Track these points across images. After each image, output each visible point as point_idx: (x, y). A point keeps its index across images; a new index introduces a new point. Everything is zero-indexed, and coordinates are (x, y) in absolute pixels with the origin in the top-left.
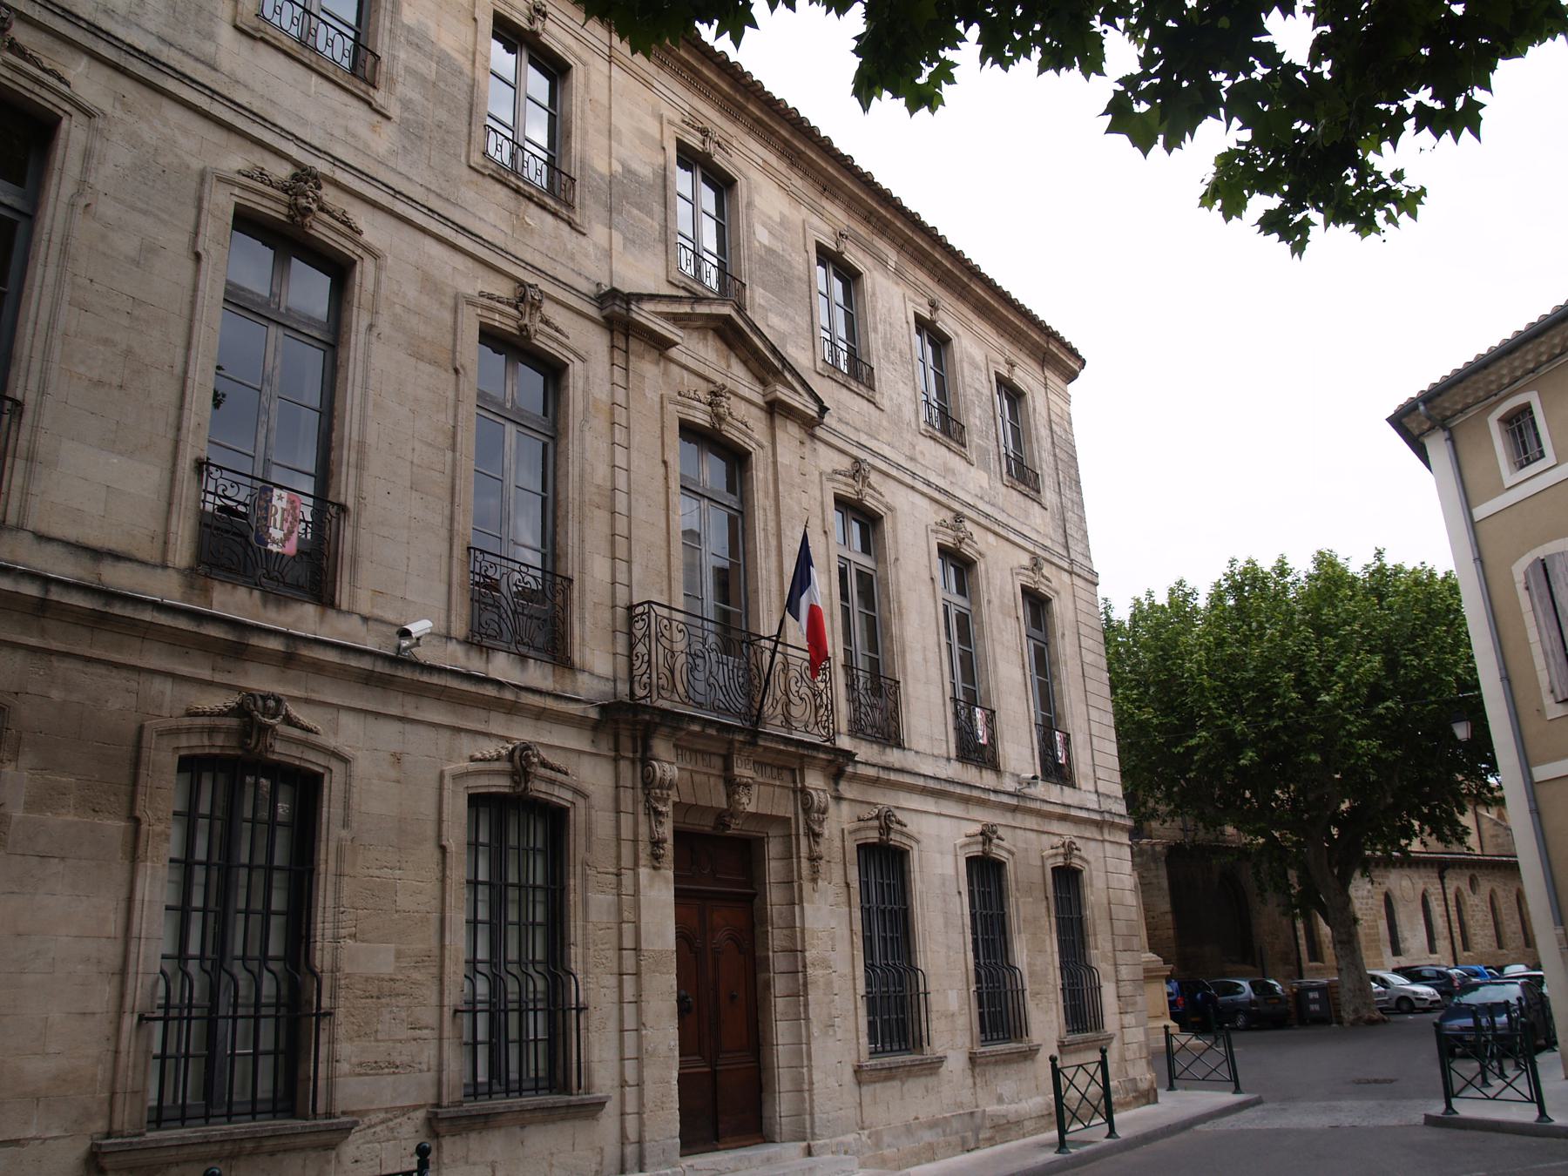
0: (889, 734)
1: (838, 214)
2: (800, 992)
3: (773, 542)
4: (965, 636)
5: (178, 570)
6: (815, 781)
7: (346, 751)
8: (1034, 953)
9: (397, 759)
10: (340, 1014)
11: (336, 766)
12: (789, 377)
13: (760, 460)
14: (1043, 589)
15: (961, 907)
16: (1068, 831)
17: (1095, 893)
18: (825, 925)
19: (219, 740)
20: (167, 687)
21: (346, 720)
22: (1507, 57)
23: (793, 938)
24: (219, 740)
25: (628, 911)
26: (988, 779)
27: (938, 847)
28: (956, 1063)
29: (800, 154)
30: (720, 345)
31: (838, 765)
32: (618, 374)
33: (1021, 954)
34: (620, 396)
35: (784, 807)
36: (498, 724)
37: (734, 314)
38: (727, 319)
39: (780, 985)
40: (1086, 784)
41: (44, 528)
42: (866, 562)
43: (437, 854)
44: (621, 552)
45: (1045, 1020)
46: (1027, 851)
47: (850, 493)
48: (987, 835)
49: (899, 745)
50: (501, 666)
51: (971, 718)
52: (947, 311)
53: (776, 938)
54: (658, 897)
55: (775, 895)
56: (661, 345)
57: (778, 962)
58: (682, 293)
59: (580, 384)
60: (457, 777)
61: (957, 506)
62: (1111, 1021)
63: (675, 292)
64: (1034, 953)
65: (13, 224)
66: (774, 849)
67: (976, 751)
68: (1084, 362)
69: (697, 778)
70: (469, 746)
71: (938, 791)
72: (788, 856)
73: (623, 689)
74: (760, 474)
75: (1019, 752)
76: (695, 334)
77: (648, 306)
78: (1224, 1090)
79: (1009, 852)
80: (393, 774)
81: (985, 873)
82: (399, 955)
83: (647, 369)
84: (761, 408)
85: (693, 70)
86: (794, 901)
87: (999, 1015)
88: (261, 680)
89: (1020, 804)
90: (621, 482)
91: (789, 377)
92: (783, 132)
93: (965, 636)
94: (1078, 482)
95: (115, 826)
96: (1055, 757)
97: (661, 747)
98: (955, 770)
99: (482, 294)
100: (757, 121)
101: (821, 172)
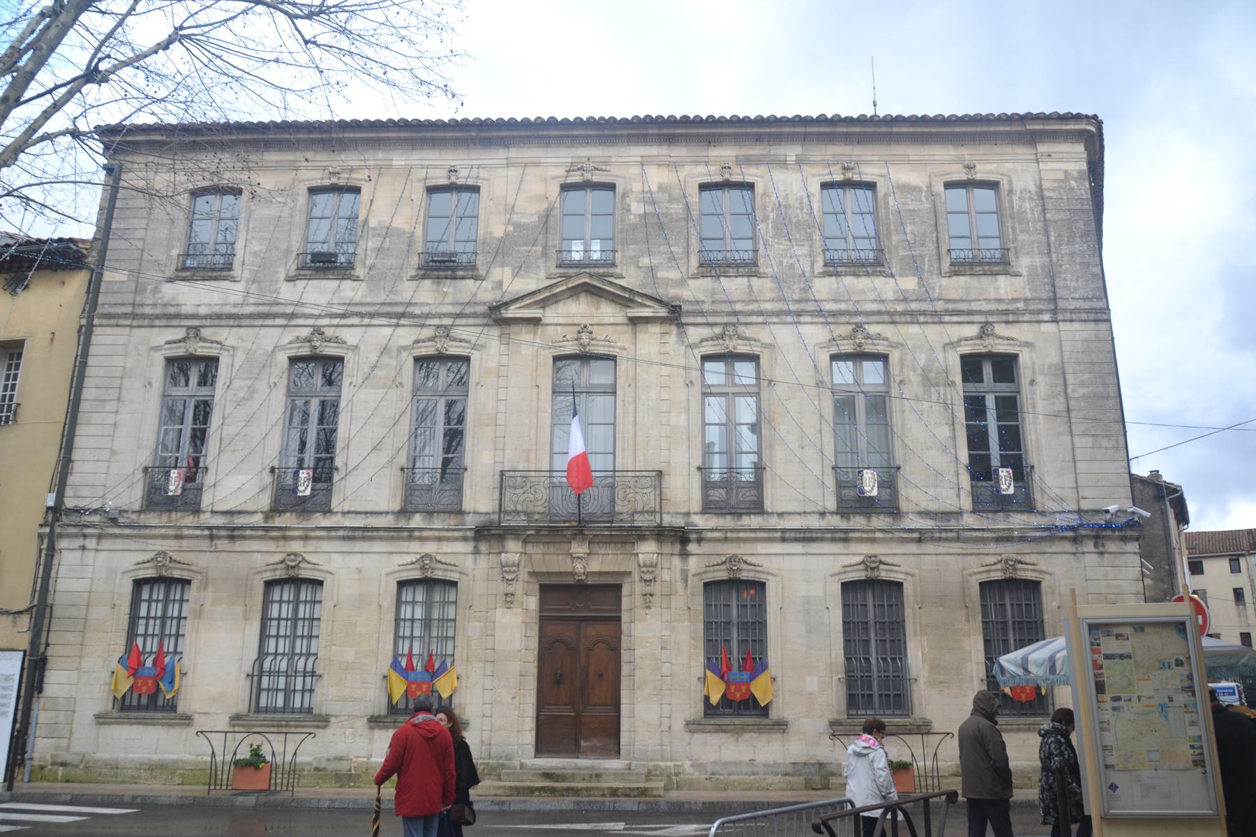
1: (819, 152)
5: (832, 513)
9: (359, 570)
19: (278, 573)
20: (258, 556)
21: (334, 556)
24: (278, 573)
29: (674, 135)
41: (780, 510)
61: (311, 322)
63: (553, 282)
65: (1015, 398)
69: (547, 557)
80: (357, 577)
82: (357, 653)
83: (524, 335)
85: (568, 136)
92: (651, 131)
99: (168, 343)
101: (698, 136)
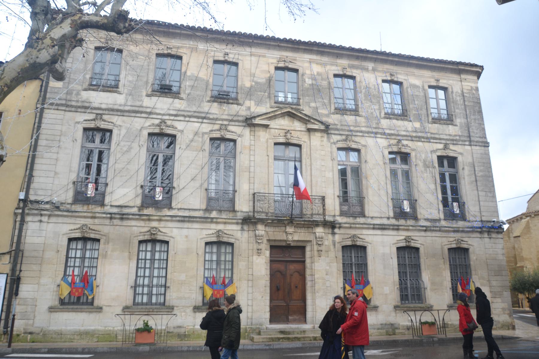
2: (313, 286)
3: (309, 168)
7: (174, 236)
9: (187, 237)
10: (171, 287)
11: (171, 239)
12: (313, 121)
16: (458, 235)
20: (136, 228)
21: (174, 230)
22: (263, 36)
23: (312, 271)
30: (289, 118)
32: (252, 138)
34: (253, 143)
36: (213, 226)
37: (290, 110)
38: (289, 112)
43: (197, 255)
44: (252, 181)
52: (400, 74)
56: (266, 126)
58: (276, 109)
59: (240, 144)
60: (201, 239)
63: (273, 110)
66: (308, 249)
68: (482, 67)
69: (275, 233)
70: (205, 232)
73: (251, 214)
76: (281, 118)
77: (257, 119)
78: (497, 336)
79: (421, 244)
82: (186, 276)
84: (306, 131)
88: (155, 224)
90: (252, 164)
91: (313, 121)
94: (480, 112)
95: (126, 254)
100: (305, 49)
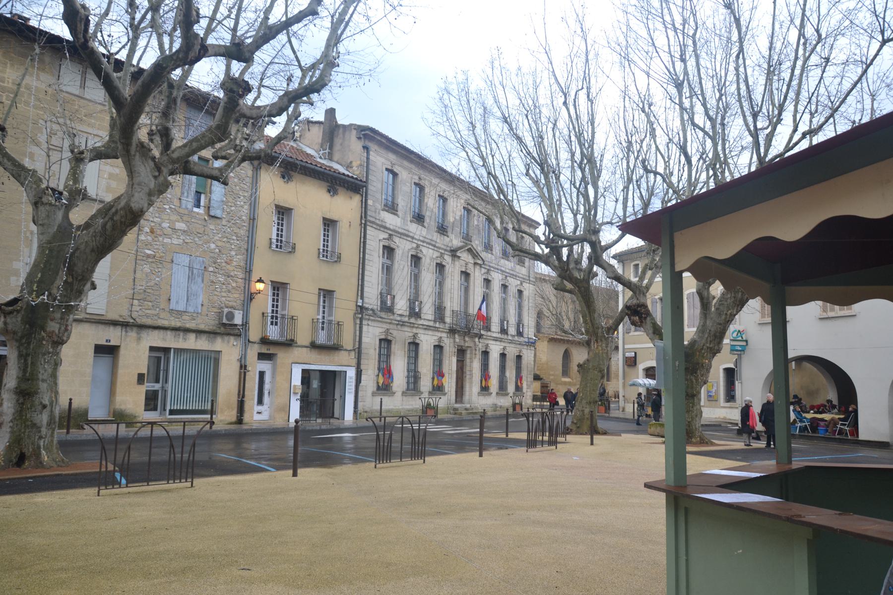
0: (488, 329)
2: (471, 378)
4: (504, 304)
6: (477, 340)
8: (511, 374)
13: (472, 275)
14: (392, 246)
15: (498, 363)
17: (524, 361)
18: (475, 366)
25: (450, 361)
26: (506, 337)
27: (495, 350)
28: (494, 394)
31: (480, 336)
33: (508, 374)
35: (471, 344)
39: (468, 377)
40: (525, 336)
42: (389, 262)
45: (511, 388)
46: (512, 351)
47: (387, 244)
48: (504, 348)
49: (490, 330)
50: (437, 325)
51: (414, 303)
53: (468, 368)
54: (454, 360)
55: (468, 361)
57: (468, 373)
62: (524, 390)
64: (511, 374)
66: (468, 352)
67: (504, 331)
71: (496, 339)
72: (471, 353)
74: (472, 278)
75: (512, 331)
81: (503, 356)
86: (471, 362)
87: (502, 387)
89: (511, 342)
93: (504, 304)
96: (414, 309)
97: (457, 336)
98: (499, 335)
